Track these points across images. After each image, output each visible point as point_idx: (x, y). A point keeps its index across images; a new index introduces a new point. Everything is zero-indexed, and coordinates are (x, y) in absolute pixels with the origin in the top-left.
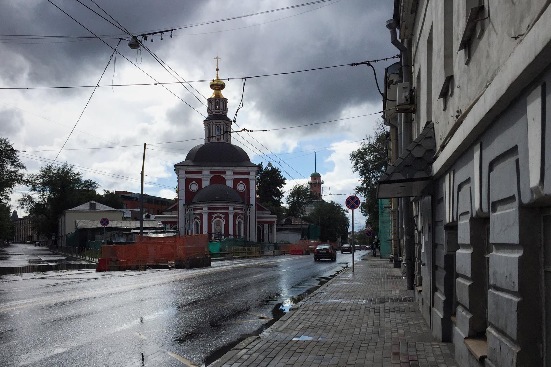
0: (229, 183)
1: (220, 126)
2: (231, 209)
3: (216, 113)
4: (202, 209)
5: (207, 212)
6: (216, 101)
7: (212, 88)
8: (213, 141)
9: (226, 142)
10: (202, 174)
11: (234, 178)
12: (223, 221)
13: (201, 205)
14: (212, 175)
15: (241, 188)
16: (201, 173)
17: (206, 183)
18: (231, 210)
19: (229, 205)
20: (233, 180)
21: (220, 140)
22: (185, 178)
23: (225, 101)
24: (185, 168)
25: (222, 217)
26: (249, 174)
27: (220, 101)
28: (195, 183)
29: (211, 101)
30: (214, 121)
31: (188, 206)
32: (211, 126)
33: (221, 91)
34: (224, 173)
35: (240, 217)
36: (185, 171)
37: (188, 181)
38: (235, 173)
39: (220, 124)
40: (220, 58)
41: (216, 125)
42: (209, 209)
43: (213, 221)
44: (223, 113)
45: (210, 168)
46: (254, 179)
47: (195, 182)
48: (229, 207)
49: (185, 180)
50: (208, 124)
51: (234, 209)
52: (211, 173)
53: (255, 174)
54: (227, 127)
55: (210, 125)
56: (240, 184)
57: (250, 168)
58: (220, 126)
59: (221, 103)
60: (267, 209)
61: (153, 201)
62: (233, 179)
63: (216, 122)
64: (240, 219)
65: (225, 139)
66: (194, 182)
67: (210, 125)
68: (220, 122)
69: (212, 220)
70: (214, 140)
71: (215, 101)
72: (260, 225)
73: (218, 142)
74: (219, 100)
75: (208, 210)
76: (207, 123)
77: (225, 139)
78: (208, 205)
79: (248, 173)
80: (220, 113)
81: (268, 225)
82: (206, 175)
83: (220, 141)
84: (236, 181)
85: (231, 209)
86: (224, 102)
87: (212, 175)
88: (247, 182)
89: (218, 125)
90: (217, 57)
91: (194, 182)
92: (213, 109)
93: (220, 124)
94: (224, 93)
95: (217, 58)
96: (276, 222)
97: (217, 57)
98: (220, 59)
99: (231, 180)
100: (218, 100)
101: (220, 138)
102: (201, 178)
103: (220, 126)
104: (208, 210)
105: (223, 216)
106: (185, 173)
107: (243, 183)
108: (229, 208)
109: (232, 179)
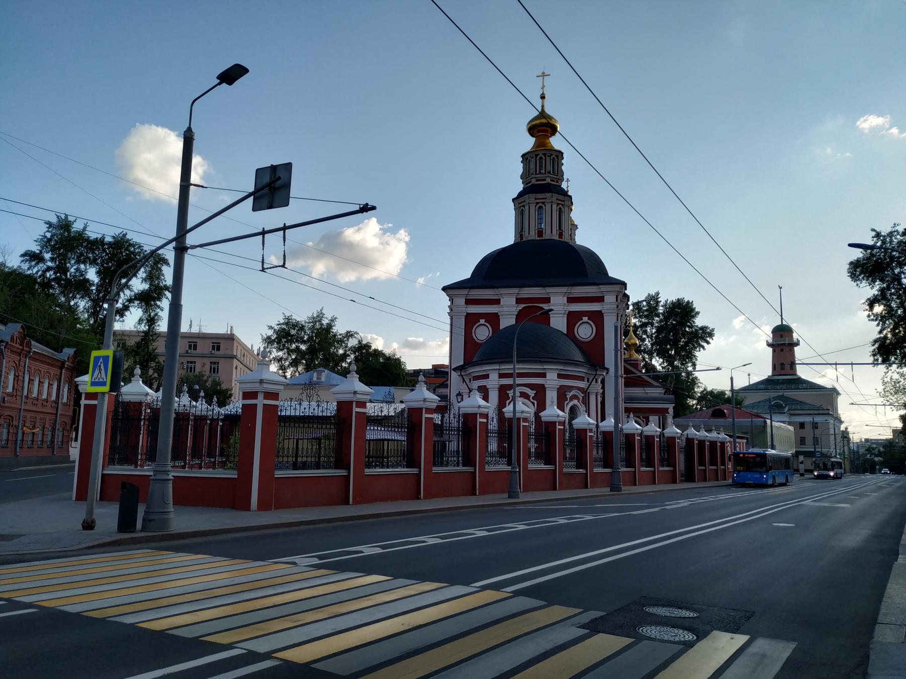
0: (559, 323)
1: (545, 205)
2: (494, 376)
3: (537, 181)
4: (486, 377)
5: (497, 383)
6: (538, 157)
7: (532, 135)
8: (529, 239)
9: (556, 238)
10: (604, 301)
11: (570, 312)
12: (643, 421)
13: (484, 369)
14: (521, 306)
15: (585, 332)
16: (497, 302)
17: (506, 322)
18: (552, 380)
19: (545, 367)
20: (566, 315)
21: (544, 235)
22: (465, 314)
23: (556, 155)
24: (465, 292)
25: (530, 394)
26: (517, 299)
27: (545, 157)
28: (587, 322)
29: (554, 156)
30: (533, 196)
31: (461, 371)
32: (527, 207)
33: (550, 139)
34: (547, 300)
35: (575, 397)
36: (464, 300)
37: (471, 320)
38: (571, 300)
39: (543, 203)
40: (548, 74)
41: (558, 204)
42: (502, 376)
43: (567, 405)
44: (551, 180)
45: (516, 291)
46: (455, 314)
47: (588, 319)
48: (547, 371)
49: (515, 317)
50: (520, 205)
51: (560, 376)
52: (519, 301)
53: (617, 300)
54: (560, 208)
55: (524, 206)
56: (583, 322)
57: (604, 288)
58: (544, 207)
59: (548, 159)
60: (655, 383)
61: (515, 359)
62: (567, 312)
63: (557, 199)
64: (575, 402)
65: (554, 232)
66: (482, 321)
67: (524, 206)
68: (545, 199)
69: (566, 402)
70: (533, 235)
71: (536, 158)
72: (639, 418)
73: (539, 239)
74: (545, 155)
75: (499, 378)
76: (519, 204)
77: (554, 232)
78: (498, 368)
79: (600, 299)
80: (545, 180)
81: (658, 417)
82: (507, 306)
83: (545, 237)
84: (573, 318)
85: (494, 376)
86: (544, 157)
87: (521, 306)
88: (597, 318)
89: (540, 204)
90: (543, 73)
91: (482, 321)
92: (532, 174)
93: (543, 203)
94: (556, 142)
95: (544, 75)
96: (671, 411)
97: (543, 73)
98: (549, 75)
99: (562, 315)
100: (543, 154)
101: (544, 231)
102: (497, 313)
103: (545, 205)
104: (499, 378)
105: (532, 393)
106: (465, 304)
107: (487, 324)
108: (547, 374)
109: (564, 314)
